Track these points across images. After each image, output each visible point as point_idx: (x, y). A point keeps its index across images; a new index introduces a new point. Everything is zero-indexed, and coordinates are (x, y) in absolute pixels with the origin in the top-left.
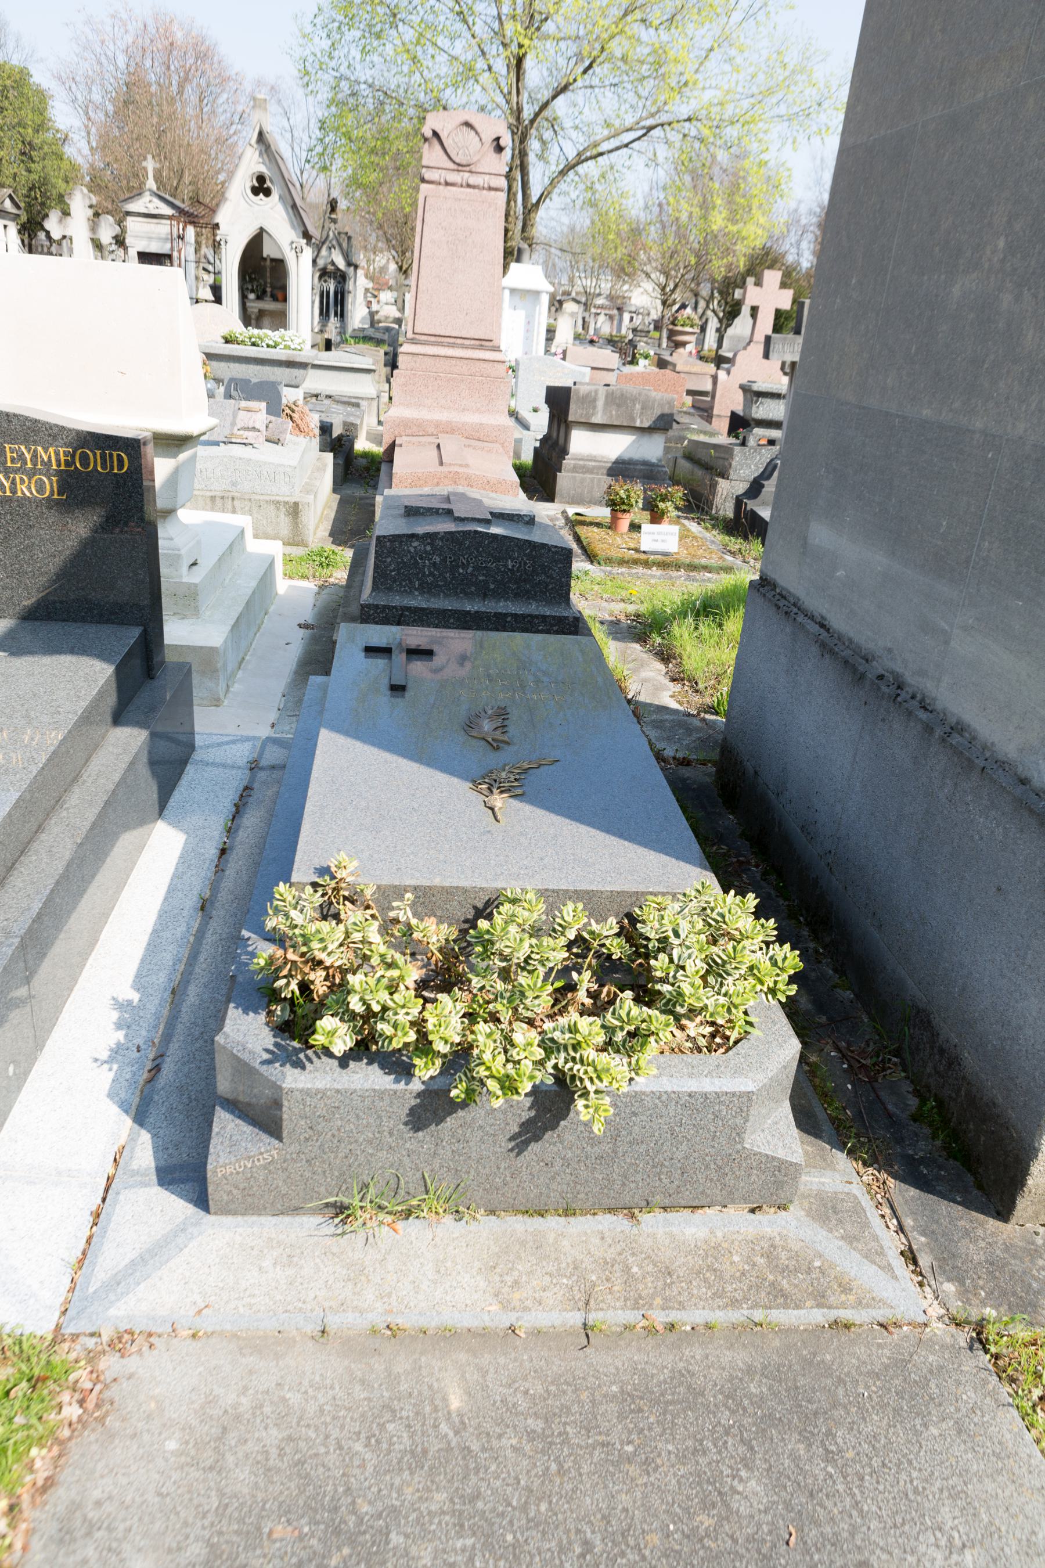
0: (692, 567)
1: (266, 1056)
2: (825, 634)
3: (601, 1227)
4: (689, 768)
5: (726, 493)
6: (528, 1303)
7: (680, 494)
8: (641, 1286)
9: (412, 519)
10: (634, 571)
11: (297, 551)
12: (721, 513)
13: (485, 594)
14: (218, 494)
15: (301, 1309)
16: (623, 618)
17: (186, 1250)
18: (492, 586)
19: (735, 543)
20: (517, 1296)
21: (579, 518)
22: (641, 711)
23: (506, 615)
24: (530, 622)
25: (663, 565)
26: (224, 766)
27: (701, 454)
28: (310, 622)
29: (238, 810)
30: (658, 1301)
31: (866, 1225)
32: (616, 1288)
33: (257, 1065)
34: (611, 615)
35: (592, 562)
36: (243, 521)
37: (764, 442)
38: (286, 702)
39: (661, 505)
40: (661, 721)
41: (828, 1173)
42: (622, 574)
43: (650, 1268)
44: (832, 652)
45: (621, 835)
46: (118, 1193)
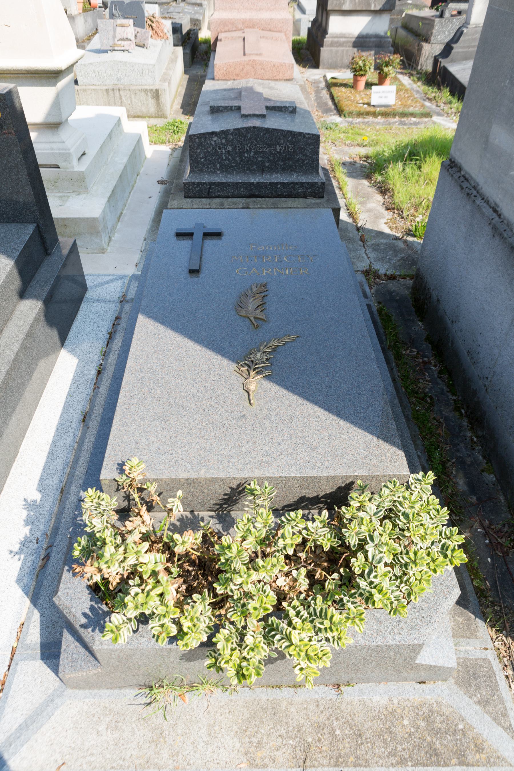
0: (404, 115)
1: (84, 621)
2: (497, 219)
3: (316, 696)
4: (394, 282)
5: (429, 51)
6: (266, 761)
7: (398, 60)
8: (341, 746)
9: (215, 115)
10: (366, 120)
11: (159, 122)
12: (424, 68)
13: (262, 170)
14: (110, 87)
15: (121, 766)
16: (357, 160)
17: (53, 718)
18: (267, 164)
19: (432, 92)
20: (259, 754)
21: (334, 81)
22: (366, 237)
23: (277, 184)
24: (293, 187)
25: (385, 115)
26: (104, 301)
27: (413, 25)
28: (165, 178)
29: (111, 336)
30: (352, 759)
31: (495, 688)
32: (324, 748)
33: (77, 627)
34: (350, 158)
35: (340, 116)
36: (119, 112)
37: (455, 13)
38: (146, 245)
39: (386, 69)
40: (378, 245)
41: (472, 641)
42: (359, 123)
43: (347, 731)
44: (501, 235)
45: (339, 414)
46: (17, 664)
